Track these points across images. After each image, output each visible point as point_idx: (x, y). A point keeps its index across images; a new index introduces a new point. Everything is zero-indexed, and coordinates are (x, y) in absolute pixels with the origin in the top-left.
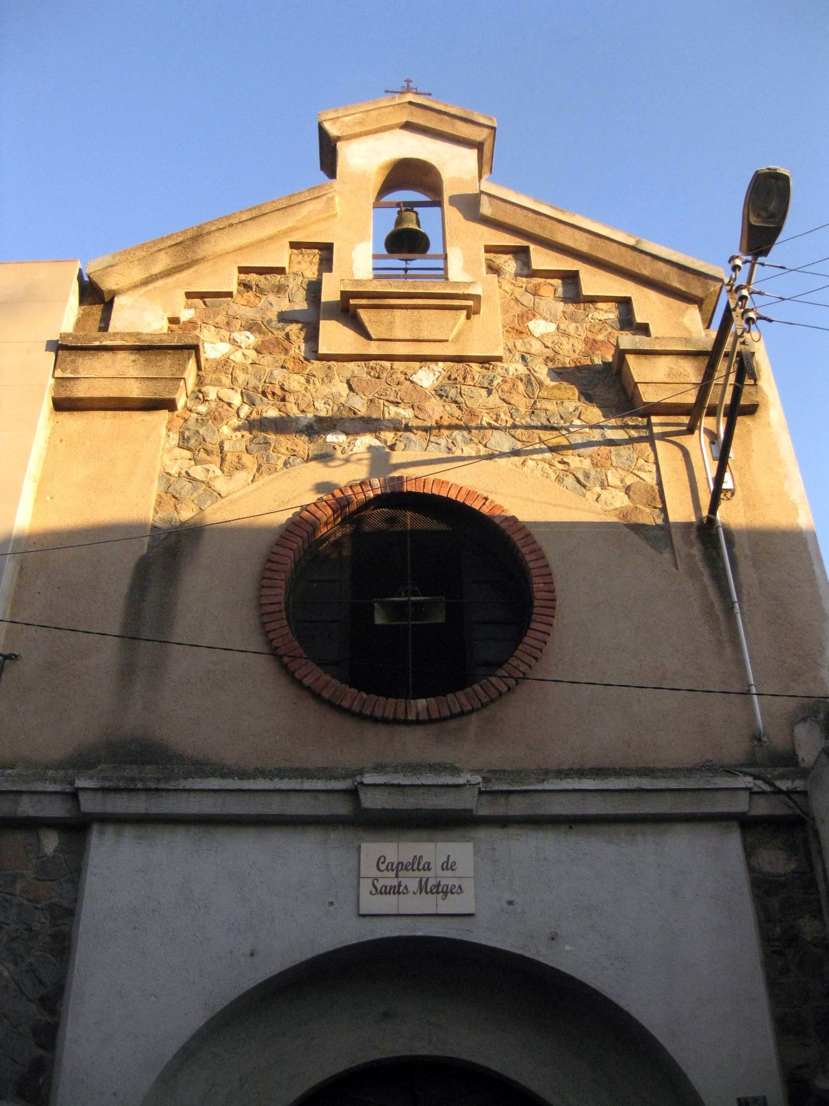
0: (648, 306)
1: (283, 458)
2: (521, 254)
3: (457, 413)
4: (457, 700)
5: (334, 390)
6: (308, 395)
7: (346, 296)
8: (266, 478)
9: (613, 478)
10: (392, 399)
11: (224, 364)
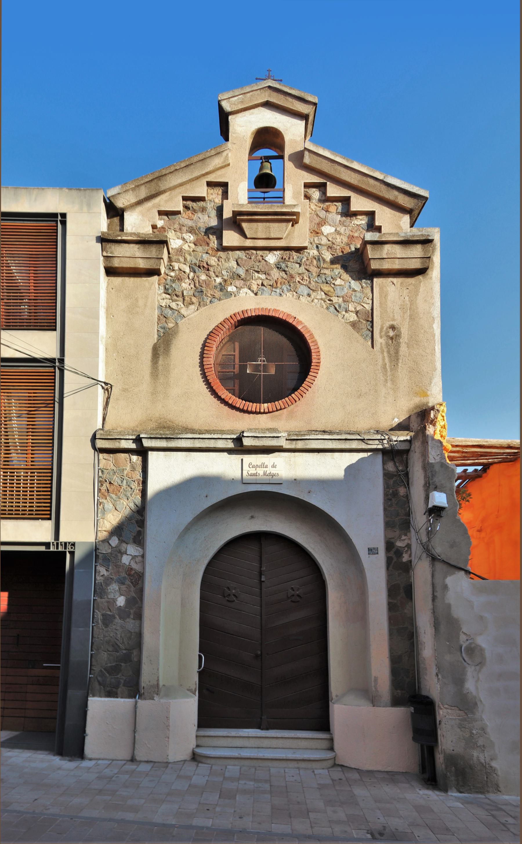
0: (385, 217)
1: (210, 299)
2: (322, 187)
3: (285, 276)
4: (279, 404)
5: (230, 265)
6: (219, 267)
7: (236, 214)
8: (202, 309)
9: (351, 307)
10: (256, 269)
11: (180, 251)
